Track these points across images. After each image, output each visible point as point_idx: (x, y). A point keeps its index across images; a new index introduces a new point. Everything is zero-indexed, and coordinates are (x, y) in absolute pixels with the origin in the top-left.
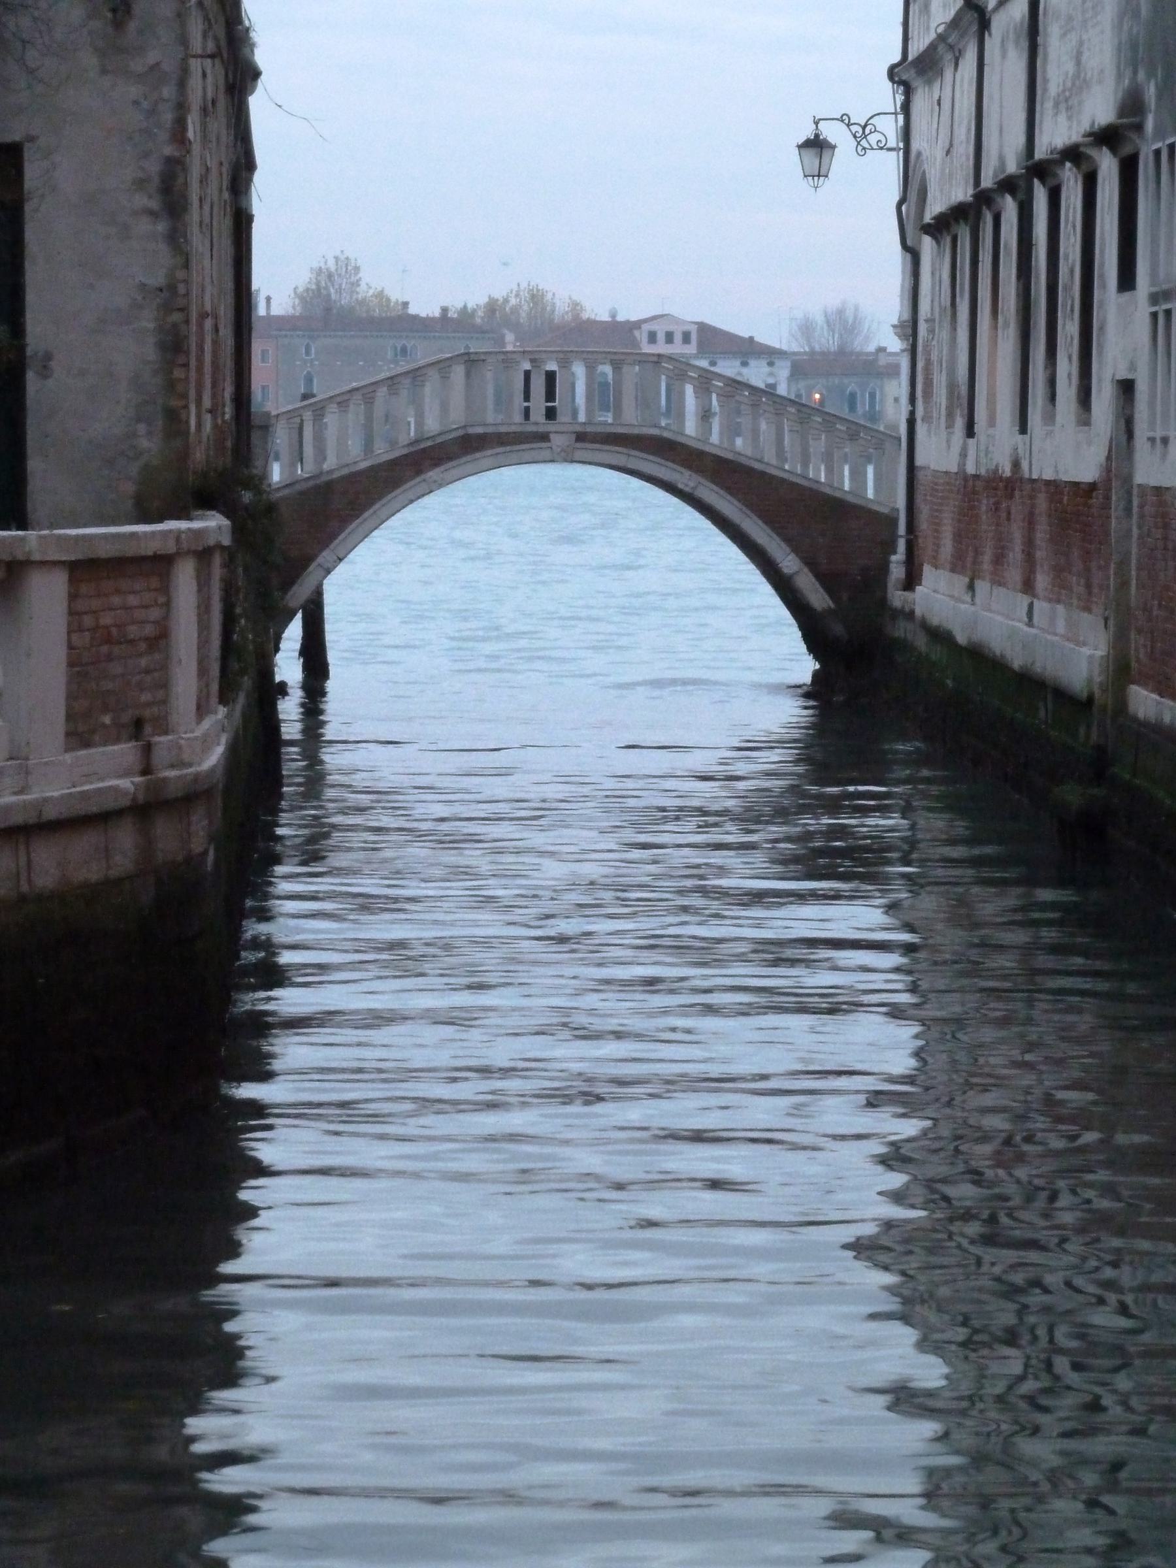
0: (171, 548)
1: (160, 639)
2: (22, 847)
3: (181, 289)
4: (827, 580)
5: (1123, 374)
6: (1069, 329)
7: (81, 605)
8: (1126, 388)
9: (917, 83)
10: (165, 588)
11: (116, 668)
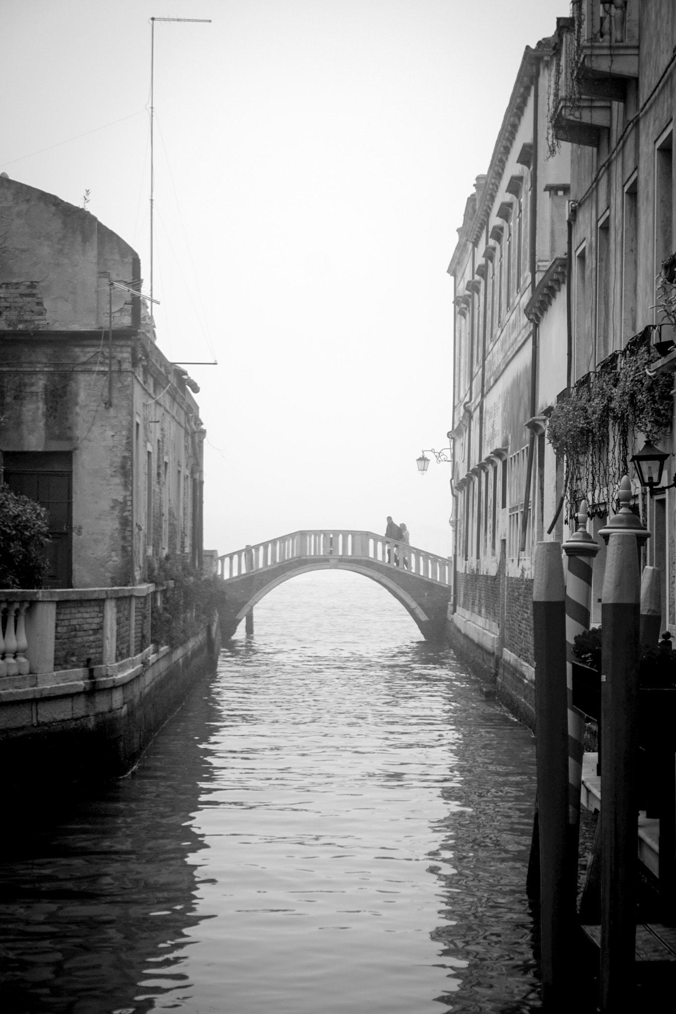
0: (103, 596)
1: (100, 628)
2: (34, 707)
3: (129, 503)
4: (426, 611)
5: (503, 538)
6: (490, 522)
7: (61, 617)
8: (504, 541)
9: (457, 438)
10: (102, 611)
11: (79, 640)
